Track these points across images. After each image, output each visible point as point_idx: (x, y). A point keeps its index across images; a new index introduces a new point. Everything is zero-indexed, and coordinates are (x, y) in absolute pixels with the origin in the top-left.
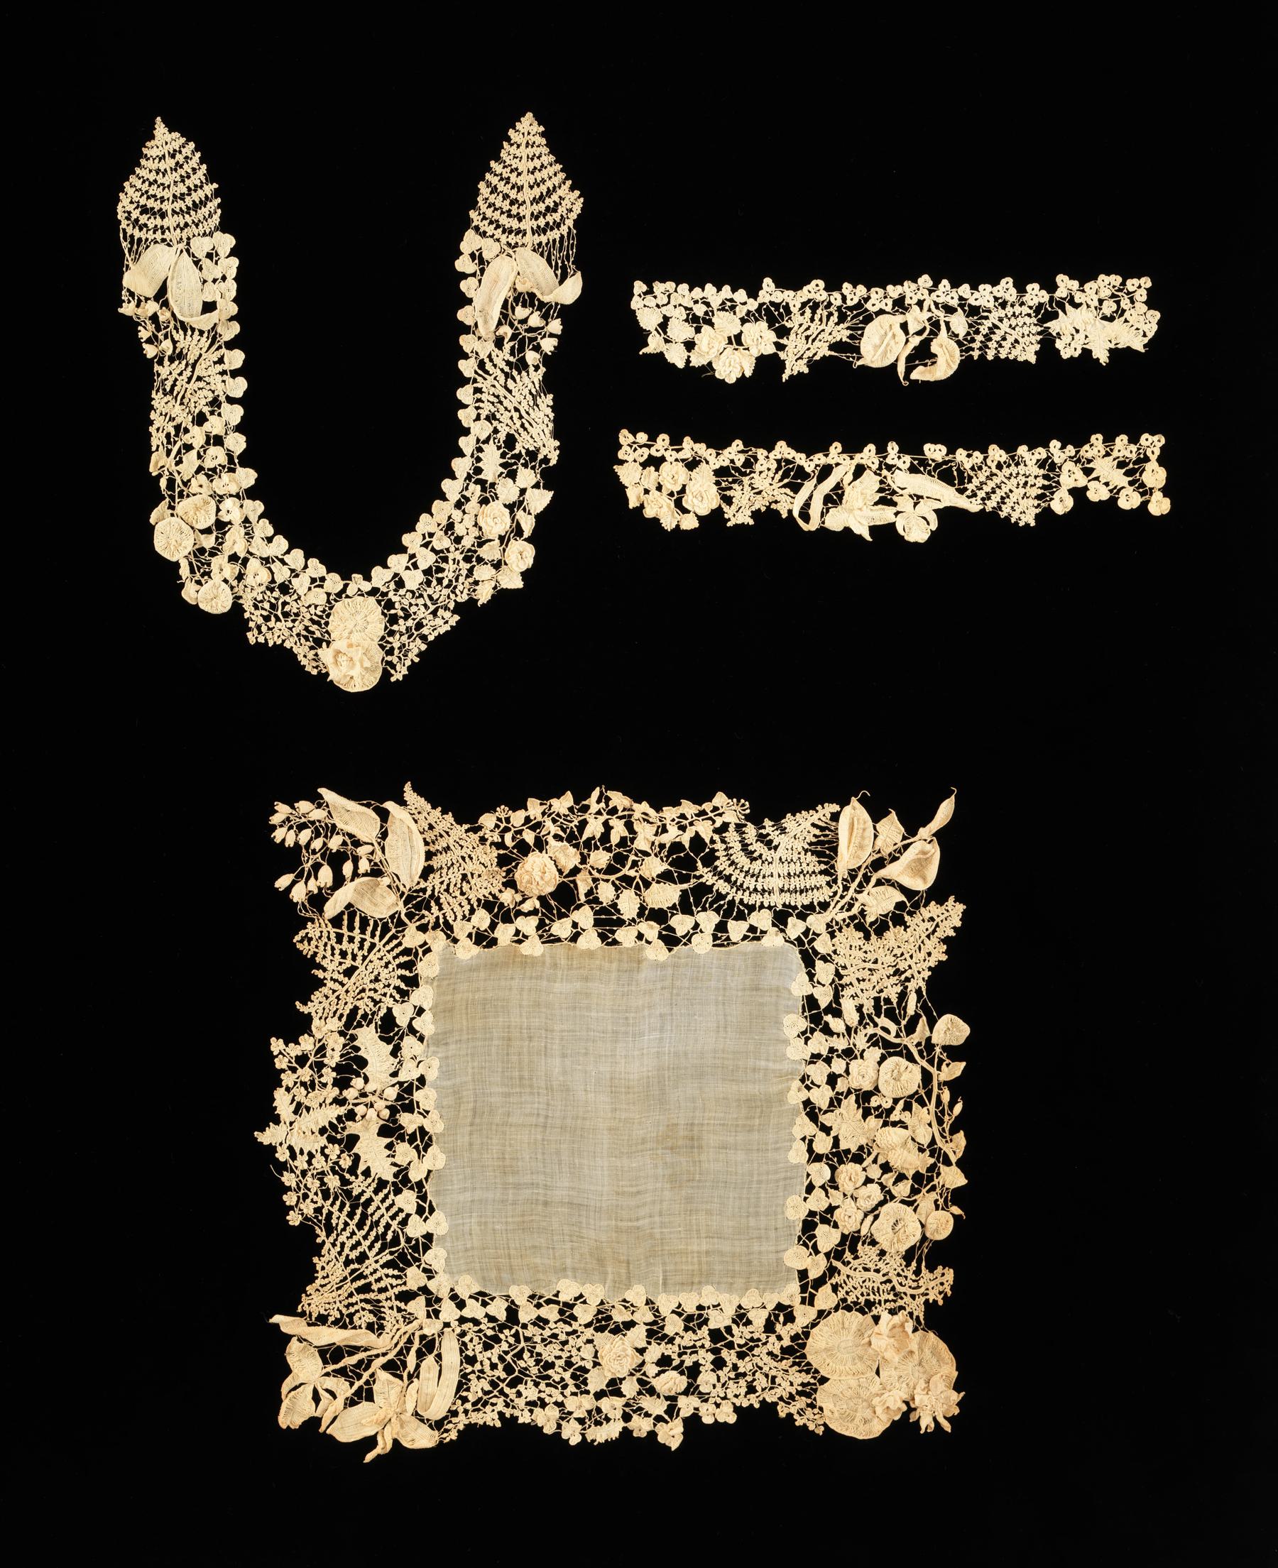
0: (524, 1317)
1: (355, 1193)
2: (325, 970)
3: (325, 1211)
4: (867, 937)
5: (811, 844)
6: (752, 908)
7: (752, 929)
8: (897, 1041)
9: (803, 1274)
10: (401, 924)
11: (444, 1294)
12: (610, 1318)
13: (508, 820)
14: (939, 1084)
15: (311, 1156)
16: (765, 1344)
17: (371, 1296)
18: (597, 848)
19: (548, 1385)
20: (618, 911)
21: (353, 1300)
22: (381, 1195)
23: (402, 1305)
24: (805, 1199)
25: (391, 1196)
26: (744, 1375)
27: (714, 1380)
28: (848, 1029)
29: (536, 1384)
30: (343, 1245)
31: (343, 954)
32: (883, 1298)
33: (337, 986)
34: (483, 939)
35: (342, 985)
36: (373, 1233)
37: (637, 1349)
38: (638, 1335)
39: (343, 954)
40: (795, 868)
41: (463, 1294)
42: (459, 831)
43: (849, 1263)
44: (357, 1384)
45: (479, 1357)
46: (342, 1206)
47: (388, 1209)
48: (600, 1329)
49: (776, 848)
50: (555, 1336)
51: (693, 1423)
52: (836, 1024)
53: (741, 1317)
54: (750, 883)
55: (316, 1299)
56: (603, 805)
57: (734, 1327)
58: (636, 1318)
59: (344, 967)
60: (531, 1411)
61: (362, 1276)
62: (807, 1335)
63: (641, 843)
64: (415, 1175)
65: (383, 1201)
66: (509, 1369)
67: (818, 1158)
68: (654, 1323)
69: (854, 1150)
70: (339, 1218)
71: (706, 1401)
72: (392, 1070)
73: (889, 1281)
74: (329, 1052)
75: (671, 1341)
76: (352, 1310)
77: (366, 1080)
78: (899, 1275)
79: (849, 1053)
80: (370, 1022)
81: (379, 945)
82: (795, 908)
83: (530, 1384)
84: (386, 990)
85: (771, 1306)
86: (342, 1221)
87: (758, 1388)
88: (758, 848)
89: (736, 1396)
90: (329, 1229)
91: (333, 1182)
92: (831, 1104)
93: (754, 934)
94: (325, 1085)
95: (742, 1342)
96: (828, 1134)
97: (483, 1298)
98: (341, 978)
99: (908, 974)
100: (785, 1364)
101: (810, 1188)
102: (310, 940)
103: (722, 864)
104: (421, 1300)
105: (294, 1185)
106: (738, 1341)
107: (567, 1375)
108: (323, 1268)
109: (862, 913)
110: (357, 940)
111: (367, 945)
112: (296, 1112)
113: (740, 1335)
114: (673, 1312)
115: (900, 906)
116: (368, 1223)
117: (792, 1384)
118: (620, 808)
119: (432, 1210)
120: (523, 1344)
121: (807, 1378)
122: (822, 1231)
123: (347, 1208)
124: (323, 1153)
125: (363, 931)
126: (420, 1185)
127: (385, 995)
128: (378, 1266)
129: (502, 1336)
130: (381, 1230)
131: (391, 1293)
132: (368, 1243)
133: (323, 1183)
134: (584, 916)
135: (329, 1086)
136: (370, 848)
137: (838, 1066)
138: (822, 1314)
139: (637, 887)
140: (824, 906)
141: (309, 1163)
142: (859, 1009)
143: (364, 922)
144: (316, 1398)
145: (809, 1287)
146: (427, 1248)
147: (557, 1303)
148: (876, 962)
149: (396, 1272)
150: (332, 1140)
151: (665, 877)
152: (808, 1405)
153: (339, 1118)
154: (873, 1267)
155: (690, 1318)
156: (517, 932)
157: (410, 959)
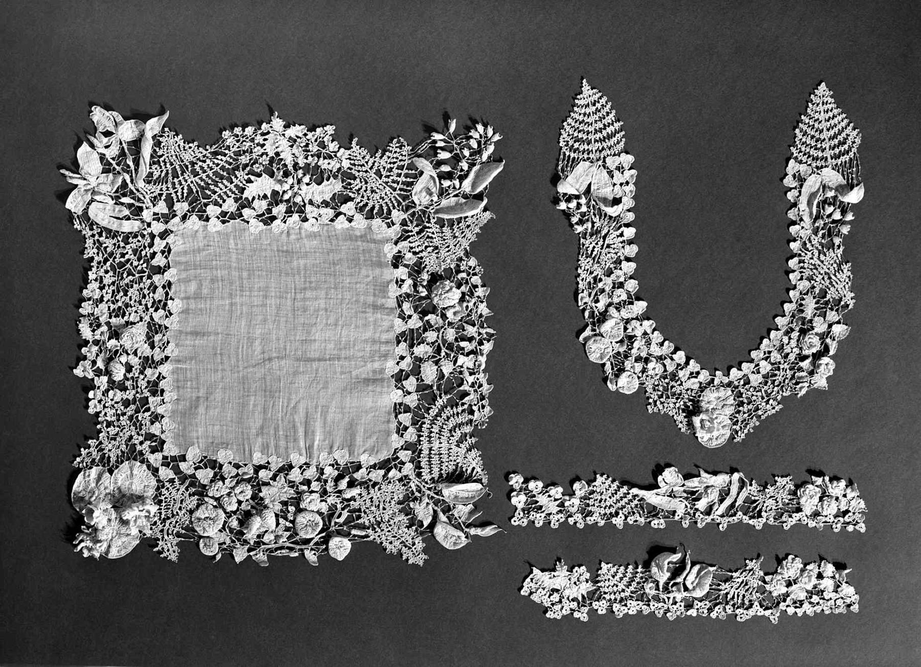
0: (156, 278)
1: (237, 172)
2: (381, 158)
3: (227, 152)
4: (399, 503)
5: (462, 467)
6: (420, 430)
7: (406, 428)
8: (333, 524)
9: (183, 458)
10: (408, 208)
11: (170, 226)
12: (157, 333)
13: (475, 274)
14: (302, 550)
15: (263, 146)
16: (138, 434)
17: (170, 178)
18: (457, 333)
19: (113, 291)
20: (419, 344)
21: (168, 165)
22: (234, 189)
23: (163, 197)
24: (230, 463)
25: (233, 196)
26: (118, 420)
27: (116, 399)
28: (340, 492)
29: (113, 283)
30: (204, 162)
31: (390, 170)
32: (163, 511)
33: (370, 164)
34: (397, 261)
35: (371, 168)
36: (210, 182)
37: (136, 350)
38: (145, 350)
39: (390, 170)
40: (445, 458)
41: (170, 239)
42: (465, 244)
43: (187, 490)
44: (113, 163)
45: (128, 247)
46: (230, 164)
47: (225, 193)
48: (149, 326)
49: (458, 446)
50: (144, 297)
51: (89, 385)
52: (343, 484)
53: (156, 418)
54: (436, 429)
55: (172, 142)
56: (485, 336)
57: (149, 413)
58: (157, 350)
59: (382, 170)
60: (96, 280)
61: (183, 172)
62: (142, 462)
63: (461, 360)
64: (246, 212)
65: (230, 190)
66: (121, 265)
67: (256, 471)
68: (153, 361)
69: (261, 495)
70: (222, 160)
71: (103, 395)
72: (314, 200)
73: (173, 516)
74: (326, 161)
75: (142, 372)
76: (162, 164)
77: (308, 184)
78: (177, 522)
79: (324, 493)
80: (345, 188)
81: (395, 194)
82: (419, 457)
83: (113, 279)
84: (366, 198)
85: (163, 437)
86: (220, 162)
87: (109, 429)
88: (458, 434)
89: (106, 414)
90: (215, 154)
91: (244, 159)
92: (290, 482)
93: (401, 430)
94: (306, 158)
95: (140, 418)
96: (271, 479)
97: (167, 251)
98: (375, 168)
99: (377, 529)
100: (123, 447)
101: (237, 466)
102: (400, 147)
103: (448, 411)
104: (166, 211)
105: (245, 133)
106: (140, 416)
107: (120, 304)
108: (190, 148)
109: (416, 499)
110: (399, 179)
111: (395, 185)
112: (290, 138)
113: (144, 417)
114: (160, 374)
115: (421, 524)
116: (217, 179)
117: (110, 450)
118: (482, 347)
119: (224, 222)
120: (137, 275)
121: (113, 459)
122: (210, 473)
123: (227, 166)
124: (263, 154)
125: (403, 183)
126: (241, 215)
127: (363, 197)
128: (189, 182)
129: (142, 262)
130: (212, 187)
131: (172, 191)
132: (204, 177)
133: (244, 152)
134: (415, 323)
135: (305, 161)
136: (458, 187)
137: (315, 486)
138: (155, 471)
139: (434, 357)
140: (419, 475)
141: (258, 144)
142: (353, 499)
143: (411, 184)
144: (108, 134)
145: (172, 462)
146: (200, 218)
147: (166, 300)
148: (384, 509)
149: (185, 195)
150: (272, 160)
151: (441, 376)
152: (94, 460)
153: (285, 165)
154: (184, 505)
155: (156, 384)
156: (403, 281)
157: (385, 215)
